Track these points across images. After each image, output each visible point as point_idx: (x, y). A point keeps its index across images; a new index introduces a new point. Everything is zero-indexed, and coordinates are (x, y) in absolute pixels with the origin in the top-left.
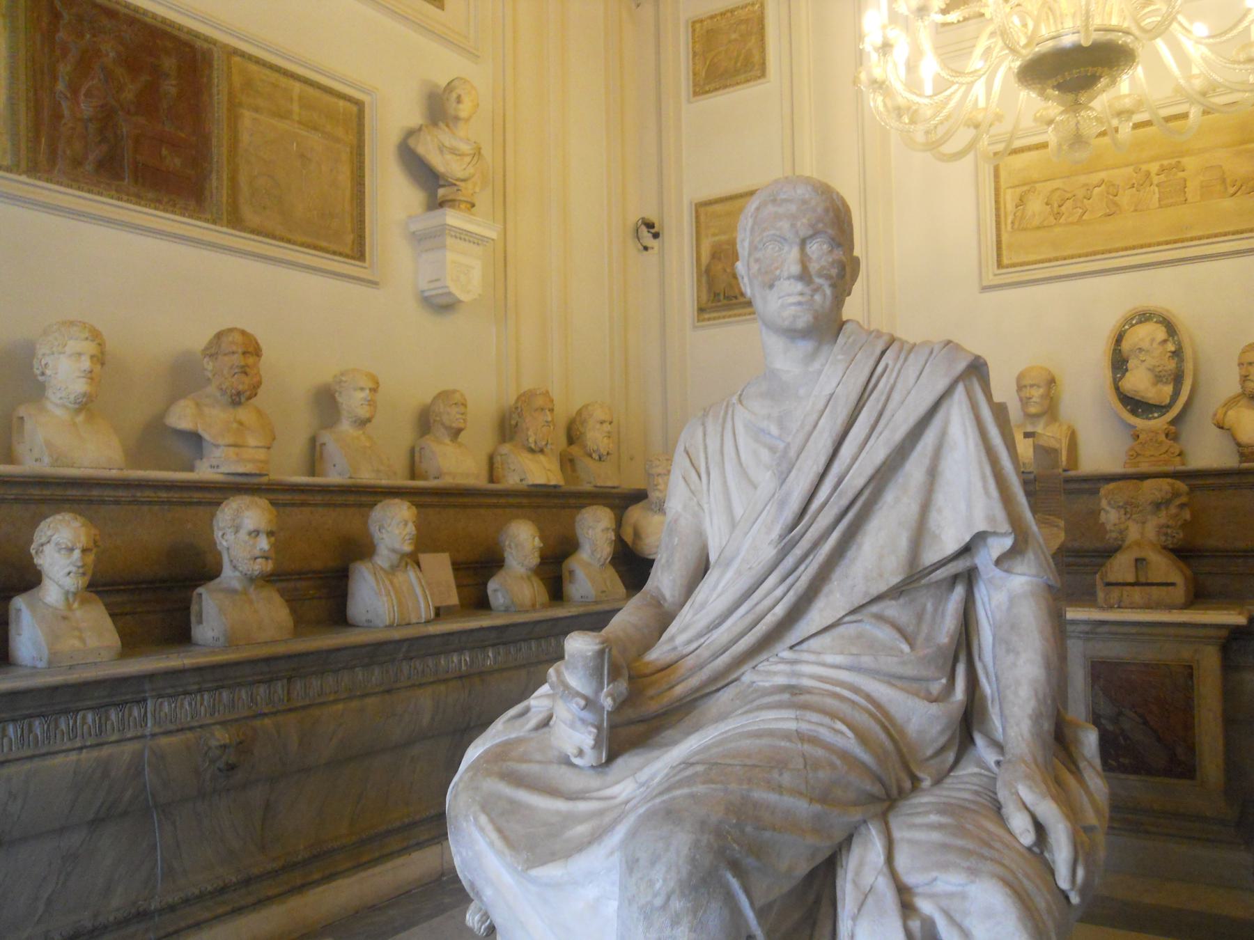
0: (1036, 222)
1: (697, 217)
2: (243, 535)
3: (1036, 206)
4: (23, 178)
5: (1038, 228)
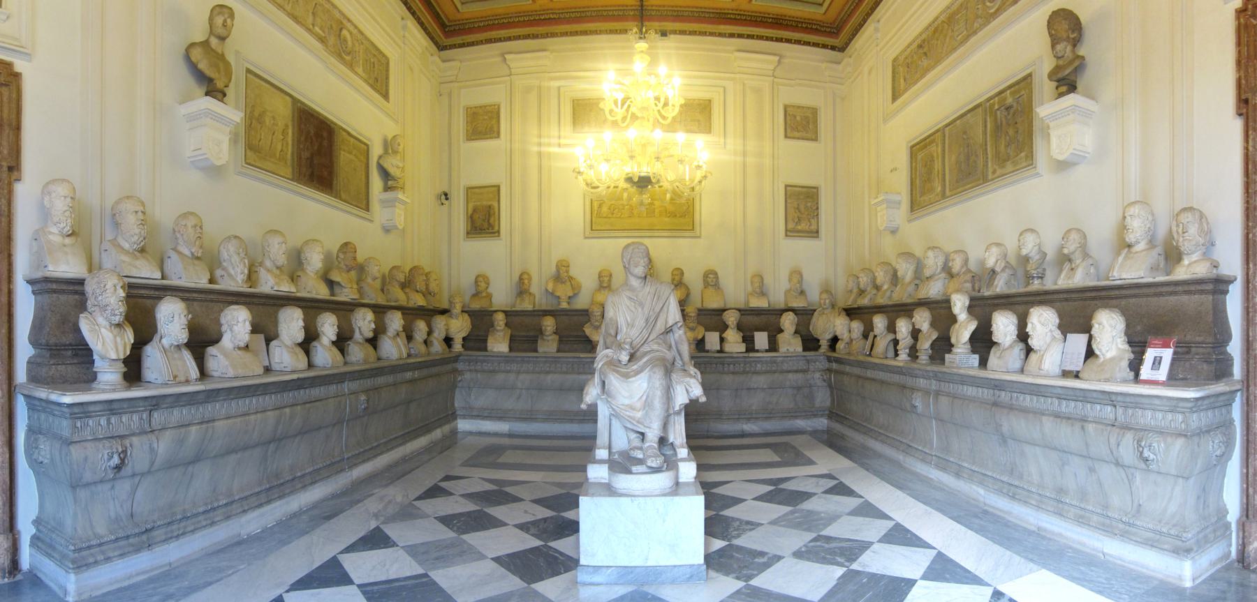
3: (605, 209)
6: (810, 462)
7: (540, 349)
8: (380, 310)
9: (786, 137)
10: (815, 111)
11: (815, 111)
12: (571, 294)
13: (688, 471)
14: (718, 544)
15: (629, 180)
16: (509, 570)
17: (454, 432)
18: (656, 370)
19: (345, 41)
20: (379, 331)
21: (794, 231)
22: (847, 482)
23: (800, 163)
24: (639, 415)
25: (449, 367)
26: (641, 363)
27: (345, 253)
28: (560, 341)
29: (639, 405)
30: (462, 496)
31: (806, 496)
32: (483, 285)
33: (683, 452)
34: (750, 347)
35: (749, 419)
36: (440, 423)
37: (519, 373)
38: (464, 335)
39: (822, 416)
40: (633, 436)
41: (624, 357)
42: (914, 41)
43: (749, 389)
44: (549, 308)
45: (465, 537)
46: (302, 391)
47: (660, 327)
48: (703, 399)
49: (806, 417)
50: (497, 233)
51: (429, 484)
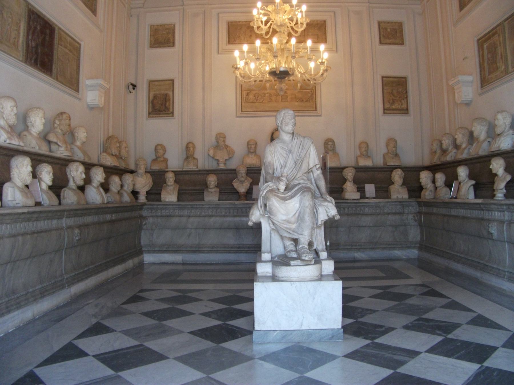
0: (251, 101)
1: (149, 85)
2: (79, 172)
3: (251, 96)
4: (24, 64)
5: (252, 102)
6: (407, 277)
8: (88, 167)
9: (381, 43)
10: (400, 25)
11: (400, 25)
12: (227, 158)
13: (329, 267)
14: (349, 321)
15: (273, 73)
16: (202, 337)
17: (142, 264)
18: (306, 194)
20: (88, 181)
21: (388, 110)
22: (438, 289)
24: (294, 226)
25: (136, 213)
27: (60, 121)
28: (220, 193)
29: (293, 220)
30: (157, 300)
31: (409, 296)
32: (161, 151)
33: (324, 255)
34: (363, 196)
35: (359, 249)
36: (132, 256)
38: (147, 189)
39: (414, 247)
41: (282, 187)
43: (359, 227)
45: (164, 323)
46: (31, 224)
48: (338, 217)
49: (402, 248)
50: (171, 114)
51: (130, 294)
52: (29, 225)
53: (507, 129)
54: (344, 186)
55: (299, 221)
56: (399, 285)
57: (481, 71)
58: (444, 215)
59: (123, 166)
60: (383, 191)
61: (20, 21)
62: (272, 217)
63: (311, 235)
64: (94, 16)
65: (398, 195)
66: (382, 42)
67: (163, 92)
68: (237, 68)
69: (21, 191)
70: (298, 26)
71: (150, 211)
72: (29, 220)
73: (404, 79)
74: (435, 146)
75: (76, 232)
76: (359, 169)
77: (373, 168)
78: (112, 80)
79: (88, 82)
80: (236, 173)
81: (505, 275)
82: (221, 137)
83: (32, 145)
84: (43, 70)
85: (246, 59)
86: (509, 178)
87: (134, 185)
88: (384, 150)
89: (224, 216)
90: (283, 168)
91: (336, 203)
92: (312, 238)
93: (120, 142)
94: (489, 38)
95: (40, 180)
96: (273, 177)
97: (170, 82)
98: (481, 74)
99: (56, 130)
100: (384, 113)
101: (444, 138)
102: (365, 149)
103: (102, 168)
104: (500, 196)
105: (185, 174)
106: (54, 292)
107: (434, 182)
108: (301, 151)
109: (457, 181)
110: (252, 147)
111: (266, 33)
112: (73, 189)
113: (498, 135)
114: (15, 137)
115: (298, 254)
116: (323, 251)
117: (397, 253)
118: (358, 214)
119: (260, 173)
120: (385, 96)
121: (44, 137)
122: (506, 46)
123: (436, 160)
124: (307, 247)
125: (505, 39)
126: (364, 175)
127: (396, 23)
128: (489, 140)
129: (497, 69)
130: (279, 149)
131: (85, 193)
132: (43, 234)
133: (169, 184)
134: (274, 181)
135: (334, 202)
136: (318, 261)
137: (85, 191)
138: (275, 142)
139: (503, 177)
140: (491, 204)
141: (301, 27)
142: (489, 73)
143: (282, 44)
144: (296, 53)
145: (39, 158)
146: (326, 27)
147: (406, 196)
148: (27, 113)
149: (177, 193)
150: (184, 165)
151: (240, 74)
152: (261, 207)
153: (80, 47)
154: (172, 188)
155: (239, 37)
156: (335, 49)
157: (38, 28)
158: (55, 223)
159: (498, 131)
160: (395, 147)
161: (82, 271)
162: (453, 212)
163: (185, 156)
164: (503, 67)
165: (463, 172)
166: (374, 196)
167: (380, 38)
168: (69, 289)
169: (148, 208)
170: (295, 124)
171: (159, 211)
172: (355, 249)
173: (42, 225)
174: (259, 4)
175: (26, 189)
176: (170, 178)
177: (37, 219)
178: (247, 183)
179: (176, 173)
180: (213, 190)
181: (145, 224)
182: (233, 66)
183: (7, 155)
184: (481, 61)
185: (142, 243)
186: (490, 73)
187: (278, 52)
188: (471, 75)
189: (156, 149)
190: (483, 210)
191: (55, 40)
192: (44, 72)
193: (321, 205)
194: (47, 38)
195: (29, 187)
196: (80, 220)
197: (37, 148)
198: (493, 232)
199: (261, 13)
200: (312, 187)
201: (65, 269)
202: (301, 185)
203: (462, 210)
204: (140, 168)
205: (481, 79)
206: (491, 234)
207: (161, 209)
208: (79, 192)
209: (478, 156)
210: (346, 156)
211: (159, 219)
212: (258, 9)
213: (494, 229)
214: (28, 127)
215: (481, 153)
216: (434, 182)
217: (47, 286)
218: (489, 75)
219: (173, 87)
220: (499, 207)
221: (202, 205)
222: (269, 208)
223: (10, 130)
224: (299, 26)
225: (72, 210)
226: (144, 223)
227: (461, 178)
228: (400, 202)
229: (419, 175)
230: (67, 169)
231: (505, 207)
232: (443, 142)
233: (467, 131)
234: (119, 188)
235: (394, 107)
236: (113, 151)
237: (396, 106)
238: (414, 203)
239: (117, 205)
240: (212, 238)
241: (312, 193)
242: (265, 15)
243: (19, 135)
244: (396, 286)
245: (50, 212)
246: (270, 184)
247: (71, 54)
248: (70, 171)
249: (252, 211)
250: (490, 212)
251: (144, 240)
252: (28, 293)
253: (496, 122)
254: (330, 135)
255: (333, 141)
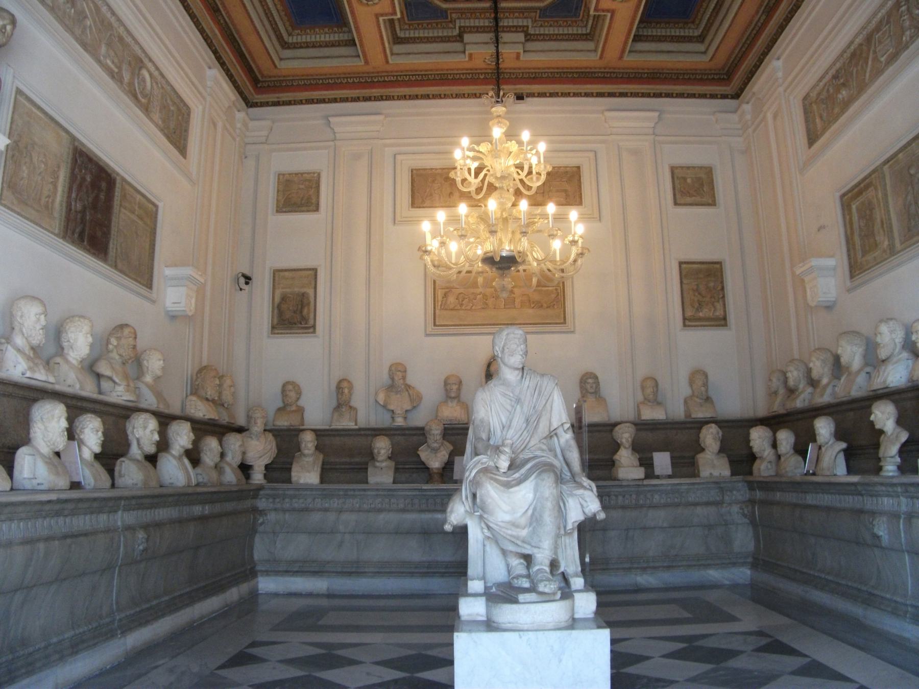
0: (451, 307)
2: (148, 431)
3: (451, 299)
4: (61, 240)
6: (732, 619)
7: (372, 479)
8: (165, 420)
9: (676, 203)
10: (709, 171)
11: (709, 171)
12: (409, 408)
13: (586, 603)
15: (489, 260)
17: (254, 595)
19: (144, 81)
20: (163, 445)
21: (690, 320)
22: (785, 639)
23: (700, 234)
24: (524, 533)
25: (248, 504)
26: (523, 471)
27: (118, 339)
28: (397, 470)
29: (523, 521)
30: (281, 661)
31: (732, 654)
32: (292, 394)
33: (578, 582)
34: (650, 474)
35: (644, 569)
37: (341, 511)
39: (743, 564)
40: (516, 562)
41: (504, 464)
42: (826, 72)
43: (644, 528)
44: (380, 426)
46: (61, 520)
47: (543, 429)
48: (602, 516)
49: (723, 566)
51: (232, 651)
52: (57, 522)
53: (897, 350)
54: (616, 457)
55: (534, 524)
56: (715, 633)
57: (848, 251)
58: (796, 505)
59: (224, 419)
60: (685, 464)
61: (59, 167)
62: (485, 516)
63: (556, 547)
64: (181, 157)
65: (712, 471)
66: (678, 202)
67: (296, 290)
68: (426, 251)
69: (46, 463)
70: (532, 179)
71: (271, 500)
72: (58, 514)
73: (718, 266)
74: (776, 383)
75: (140, 536)
76: (641, 426)
77: (667, 423)
78: (210, 268)
79: (168, 272)
80: (424, 434)
81: (906, 612)
82: (398, 371)
83: (69, 382)
84: (93, 251)
85: (442, 237)
86: (904, 436)
87: (244, 453)
88: (686, 391)
89: (404, 511)
90: (506, 429)
91: (597, 487)
92: (556, 553)
93: (221, 378)
94: (860, 193)
95: (81, 443)
96: (488, 447)
97: (310, 272)
98: (849, 255)
99: (111, 355)
100: (685, 325)
101: (791, 368)
102: (652, 390)
103: (189, 424)
104: (890, 468)
105: (334, 436)
106: (95, 645)
107: (774, 445)
108: (537, 400)
109: (815, 444)
110: (453, 390)
111: (476, 189)
112: (138, 461)
113: (883, 361)
114: (41, 367)
115: (532, 582)
116: (576, 575)
117: (714, 574)
118: (642, 506)
119: (467, 434)
120: (685, 295)
121: (90, 367)
122: (888, 207)
123: (778, 408)
124: (547, 569)
125: (886, 195)
126: (651, 437)
127: (701, 168)
128: (868, 369)
129: (876, 245)
130: (499, 396)
131: (158, 467)
132: (82, 538)
133: (306, 452)
134: (489, 453)
135: (595, 489)
136: (567, 594)
137: (158, 463)
138: (492, 383)
139: (895, 435)
140: (875, 484)
141: (538, 179)
142: (865, 250)
143: (504, 210)
144: (528, 225)
145: (79, 404)
146: (580, 177)
147: (727, 472)
148: (62, 326)
149: (319, 469)
150: (332, 418)
151: (432, 261)
152: (467, 498)
153: (157, 210)
154: (311, 459)
155: (431, 195)
156: (596, 215)
157: (88, 179)
158: (103, 519)
159: (883, 354)
160: (705, 385)
161: (148, 606)
162: (810, 499)
163: (334, 403)
164: (886, 243)
165: (824, 428)
166: (670, 472)
167: (674, 195)
168: (122, 640)
169: (267, 495)
170: (526, 353)
171: (287, 500)
172: (637, 568)
173: (81, 522)
174: (465, 141)
175: (55, 460)
176: (308, 441)
177: (73, 513)
178: (444, 452)
179: (319, 433)
180: (384, 464)
181: (261, 524)
182: (419, 249)
183: (24, 398)
184: (849, 232)
185: (256, 556)
186: (865, 252)
187: (496, 225)
188: (832, 256)
189: (283, 391)
190: (862, 495)
191: (116, 198)
192: (94, 255)
193: (572, 495)
194: (102, 196)
195: (62, 455)
196: (148, 516)
197: (78, 386)
198: (881, 533)
199: (468, 157)
200: (556, 463)
201: (117, 603)
202: (537, 460)
203: (826, 496)
204: (256, 423)
205: (850, 263)
206: (878, 537)
207: (292, 497)
208: (147, 464)
209: (850, 398)
210: (619, 403)
211: (287, 516)
212: (463, 149)
213: (882, 529)
214: (63, 349)
215: (855, 393)
216: (774, 445)
217: (84, 632)
218: (863, 256)
219: (316, 282)
220: (890, 489)
221: (364, 490)
222: (482, 500)
223: (32, 355)
224: (534, 178)
225: (133, 497)
226: (261, 520)
227: (822, 438)
228: (716, 483)
229: (748, 434)
230: (127, 424)
231: (899, 489)
232: (789, 375)
233: (829, 354)
234: (217, 459)
235: (701, 314)
236: (209, 393)
237: (705, 313)
238: (740, 484)
239: (213, 489)
240: (379, 551)
241: (556, 474)
242: (474, 159)
243: (48, 363)
244: (711, 635)
245: (95, 499)
246: (483, 458)
247: (140, 222)
248: (134, 428)
249: (450, 505)
250: (874, 499)
251: (260, 550)
252: (50, 645)
253: (879, 339)
254: (588, 365)
255: (596, 377)
